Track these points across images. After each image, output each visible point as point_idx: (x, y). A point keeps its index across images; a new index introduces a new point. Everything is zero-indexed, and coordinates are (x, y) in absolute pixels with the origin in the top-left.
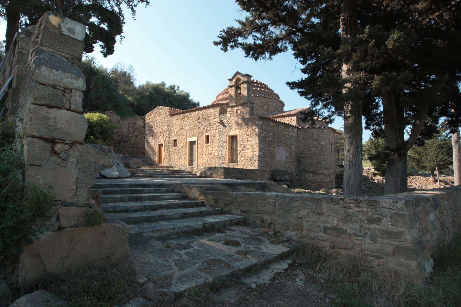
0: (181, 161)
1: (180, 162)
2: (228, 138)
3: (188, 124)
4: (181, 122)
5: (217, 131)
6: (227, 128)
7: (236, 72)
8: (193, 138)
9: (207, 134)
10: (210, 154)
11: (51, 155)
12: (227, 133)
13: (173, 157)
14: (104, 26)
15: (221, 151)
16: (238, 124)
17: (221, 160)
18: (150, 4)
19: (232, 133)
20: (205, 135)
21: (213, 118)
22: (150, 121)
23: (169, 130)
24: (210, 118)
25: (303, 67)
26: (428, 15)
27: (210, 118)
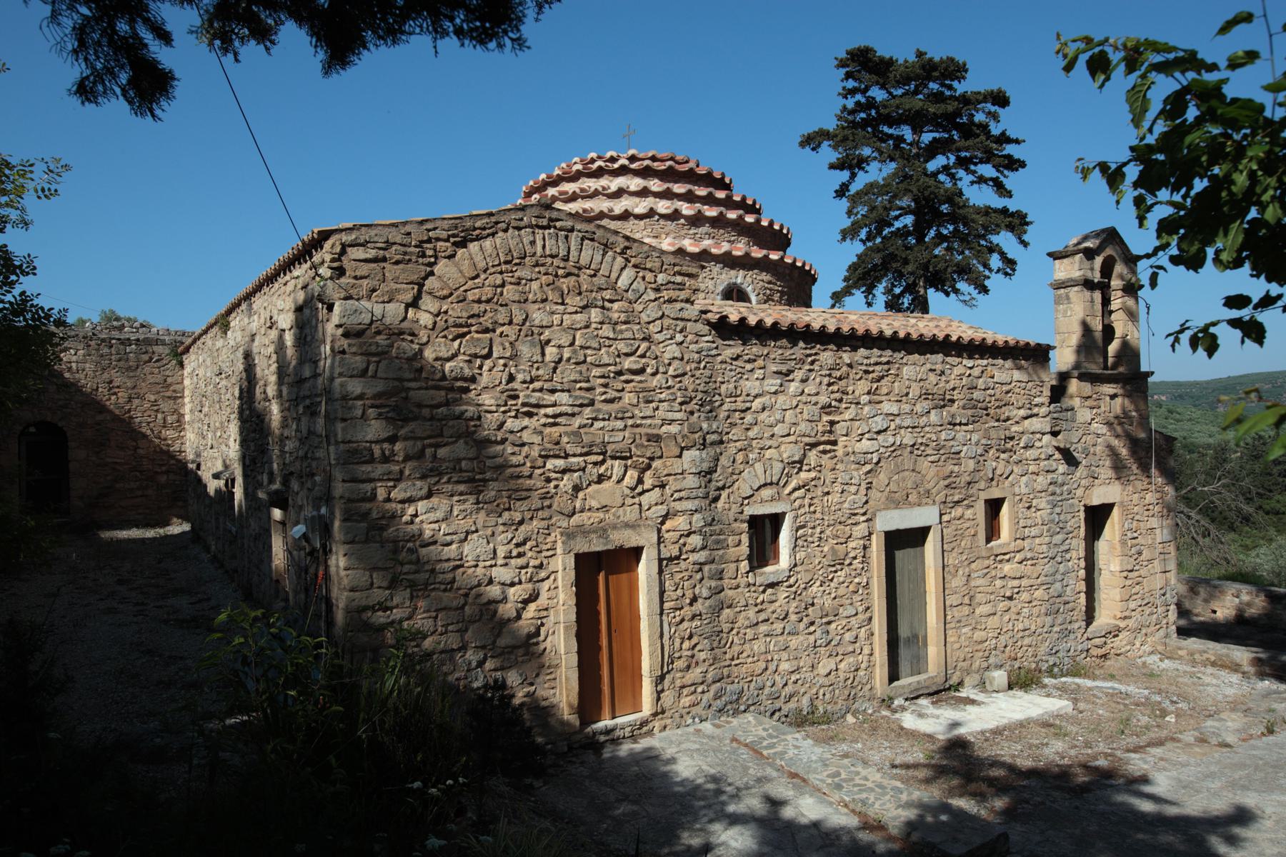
0: (825, 665)
1: (822, 670)
2: (1082, 515)
3: (879, 423)
4: (823, 399)
5: (1042, 481)
6: (1081, 471)
7: (1109, 225)
8: (917, 510)
9: (995, 493)
10: (1010, 598)
11: (423, 308)
12: (1079, 492)
13: (758, 646)
14: (1182, 231)
15: (1059, 577)
16: (1119, 467)
17: (1060, 620)
18: (1131, 125)
19: (1097, 497)
20: (984, 496)
21: (1022, 412)
22: (425, 319)
23: (712, 443)
24: (1006, 412)
25: (27, 284)
26: (337, 396)
27: (1006, 412)
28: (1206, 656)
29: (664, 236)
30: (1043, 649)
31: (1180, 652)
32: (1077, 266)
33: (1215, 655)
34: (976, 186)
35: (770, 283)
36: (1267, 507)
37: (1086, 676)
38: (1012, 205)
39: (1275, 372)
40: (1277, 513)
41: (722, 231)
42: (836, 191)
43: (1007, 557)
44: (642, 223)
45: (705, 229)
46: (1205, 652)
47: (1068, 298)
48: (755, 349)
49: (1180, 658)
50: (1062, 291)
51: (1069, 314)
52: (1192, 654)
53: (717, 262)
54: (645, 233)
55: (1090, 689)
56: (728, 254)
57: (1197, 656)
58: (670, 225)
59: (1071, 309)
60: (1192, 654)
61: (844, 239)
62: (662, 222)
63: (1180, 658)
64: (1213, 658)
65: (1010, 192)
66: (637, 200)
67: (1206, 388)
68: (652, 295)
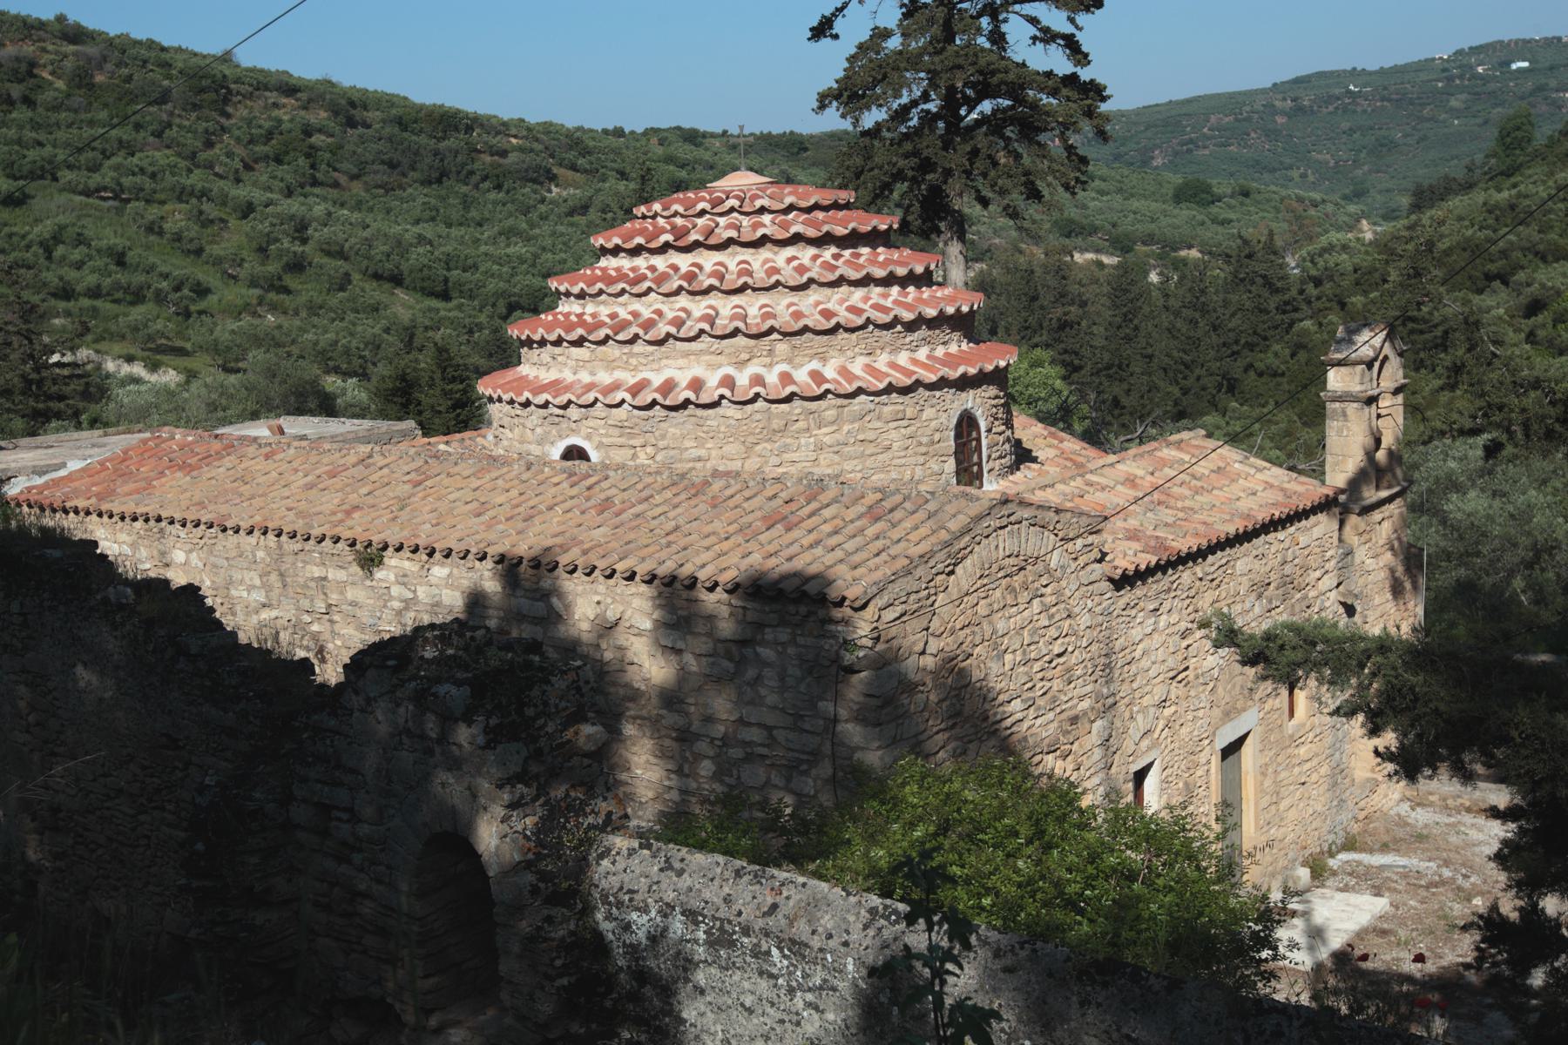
28: (1460, 801)
29: (879, 352)
30: (1325, 829)
31: (1432, 798)
32: (1357, 379)
33: (1470, 800)
34: (1040, 46)
35: (997, 397)
36: (1260, 365)
37: (1362, 850)
38: (1085, 74)
39: (1240, 93)
40: (1275, 375)
41: (937, 332)
42: (812, 29)
43: (969, 549)
44: (854, 336)
45: (923, 332)
46: (1459, 797)
47: (1344, 414)
48: (1139, 591)
49: (1431, 804)
50: (1337, 404)
51: (1345, 433)
52: (1445, 800)
53: (950, 387)
54: (857, 350)
55: (1382, 868)
56: (964, 376)
57: (1450, 802)
58: (886, 335)
59: (1348, 428)
60: (1445, 800)
61: (822, 106)
62: (877, 332)
63: (1431, 804)
64: (1468, 804)
65: (1086, 55)
66: (828, 291)
67: (1135, 124)
68: (1073, 565)
